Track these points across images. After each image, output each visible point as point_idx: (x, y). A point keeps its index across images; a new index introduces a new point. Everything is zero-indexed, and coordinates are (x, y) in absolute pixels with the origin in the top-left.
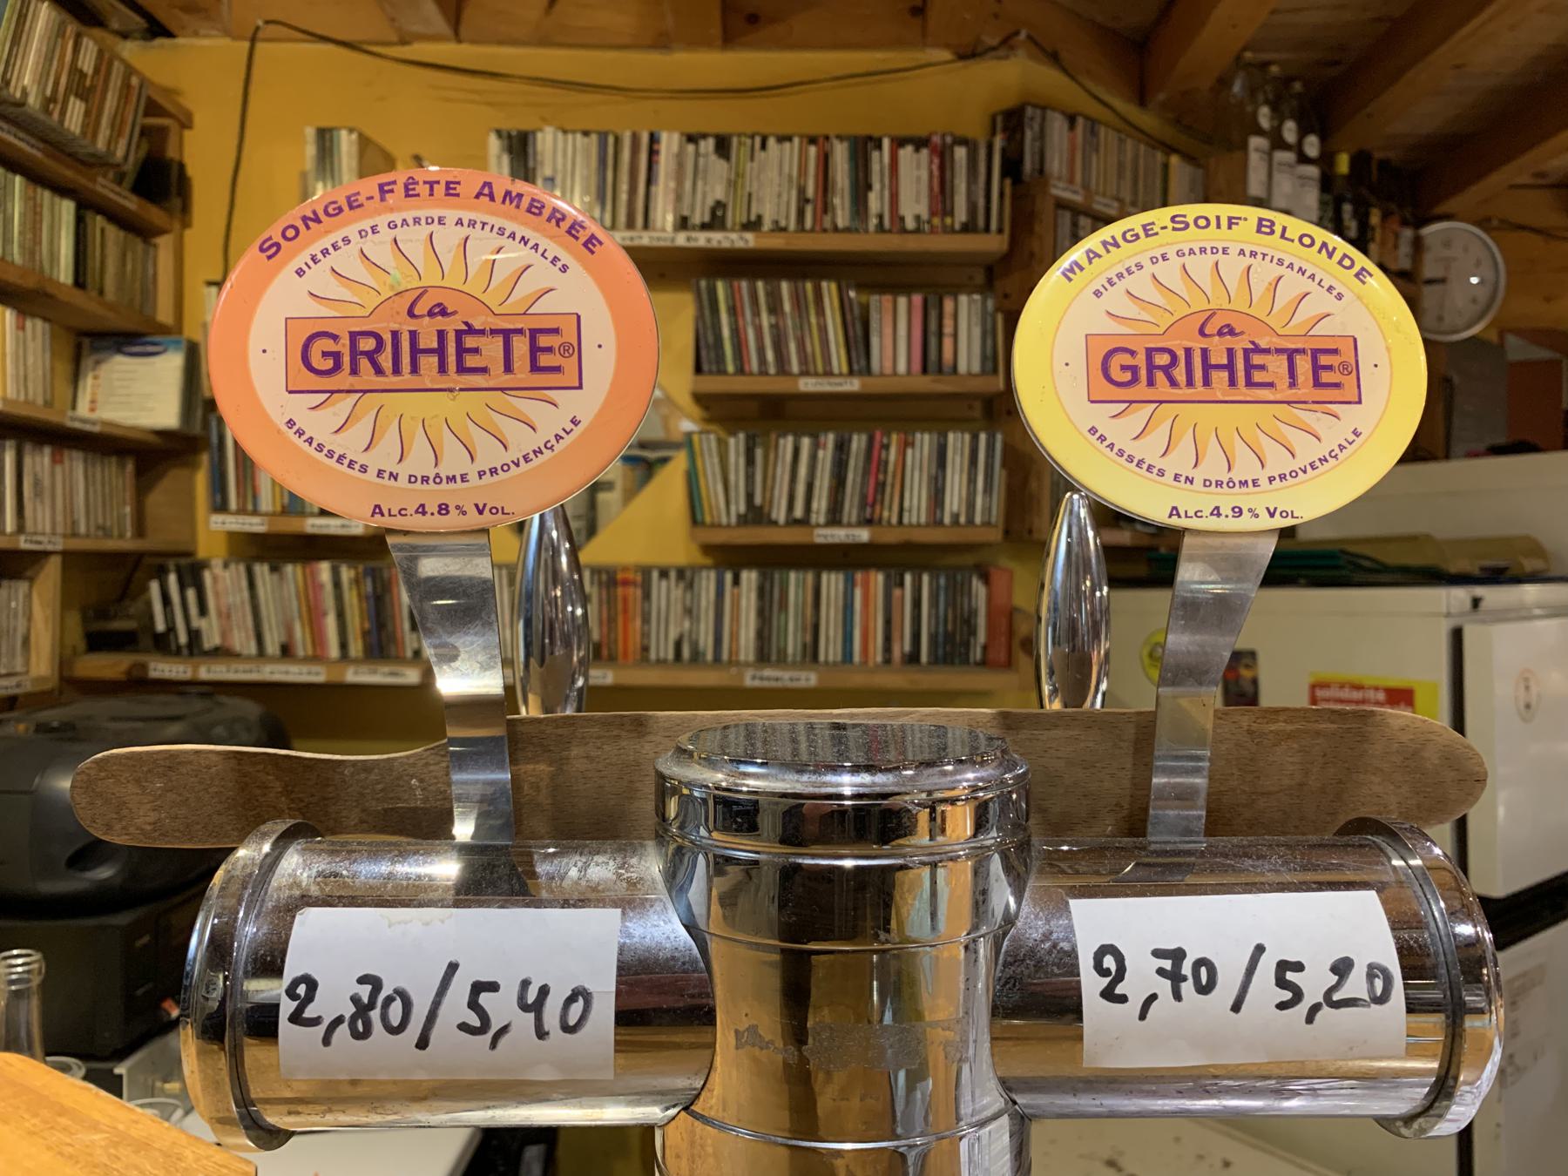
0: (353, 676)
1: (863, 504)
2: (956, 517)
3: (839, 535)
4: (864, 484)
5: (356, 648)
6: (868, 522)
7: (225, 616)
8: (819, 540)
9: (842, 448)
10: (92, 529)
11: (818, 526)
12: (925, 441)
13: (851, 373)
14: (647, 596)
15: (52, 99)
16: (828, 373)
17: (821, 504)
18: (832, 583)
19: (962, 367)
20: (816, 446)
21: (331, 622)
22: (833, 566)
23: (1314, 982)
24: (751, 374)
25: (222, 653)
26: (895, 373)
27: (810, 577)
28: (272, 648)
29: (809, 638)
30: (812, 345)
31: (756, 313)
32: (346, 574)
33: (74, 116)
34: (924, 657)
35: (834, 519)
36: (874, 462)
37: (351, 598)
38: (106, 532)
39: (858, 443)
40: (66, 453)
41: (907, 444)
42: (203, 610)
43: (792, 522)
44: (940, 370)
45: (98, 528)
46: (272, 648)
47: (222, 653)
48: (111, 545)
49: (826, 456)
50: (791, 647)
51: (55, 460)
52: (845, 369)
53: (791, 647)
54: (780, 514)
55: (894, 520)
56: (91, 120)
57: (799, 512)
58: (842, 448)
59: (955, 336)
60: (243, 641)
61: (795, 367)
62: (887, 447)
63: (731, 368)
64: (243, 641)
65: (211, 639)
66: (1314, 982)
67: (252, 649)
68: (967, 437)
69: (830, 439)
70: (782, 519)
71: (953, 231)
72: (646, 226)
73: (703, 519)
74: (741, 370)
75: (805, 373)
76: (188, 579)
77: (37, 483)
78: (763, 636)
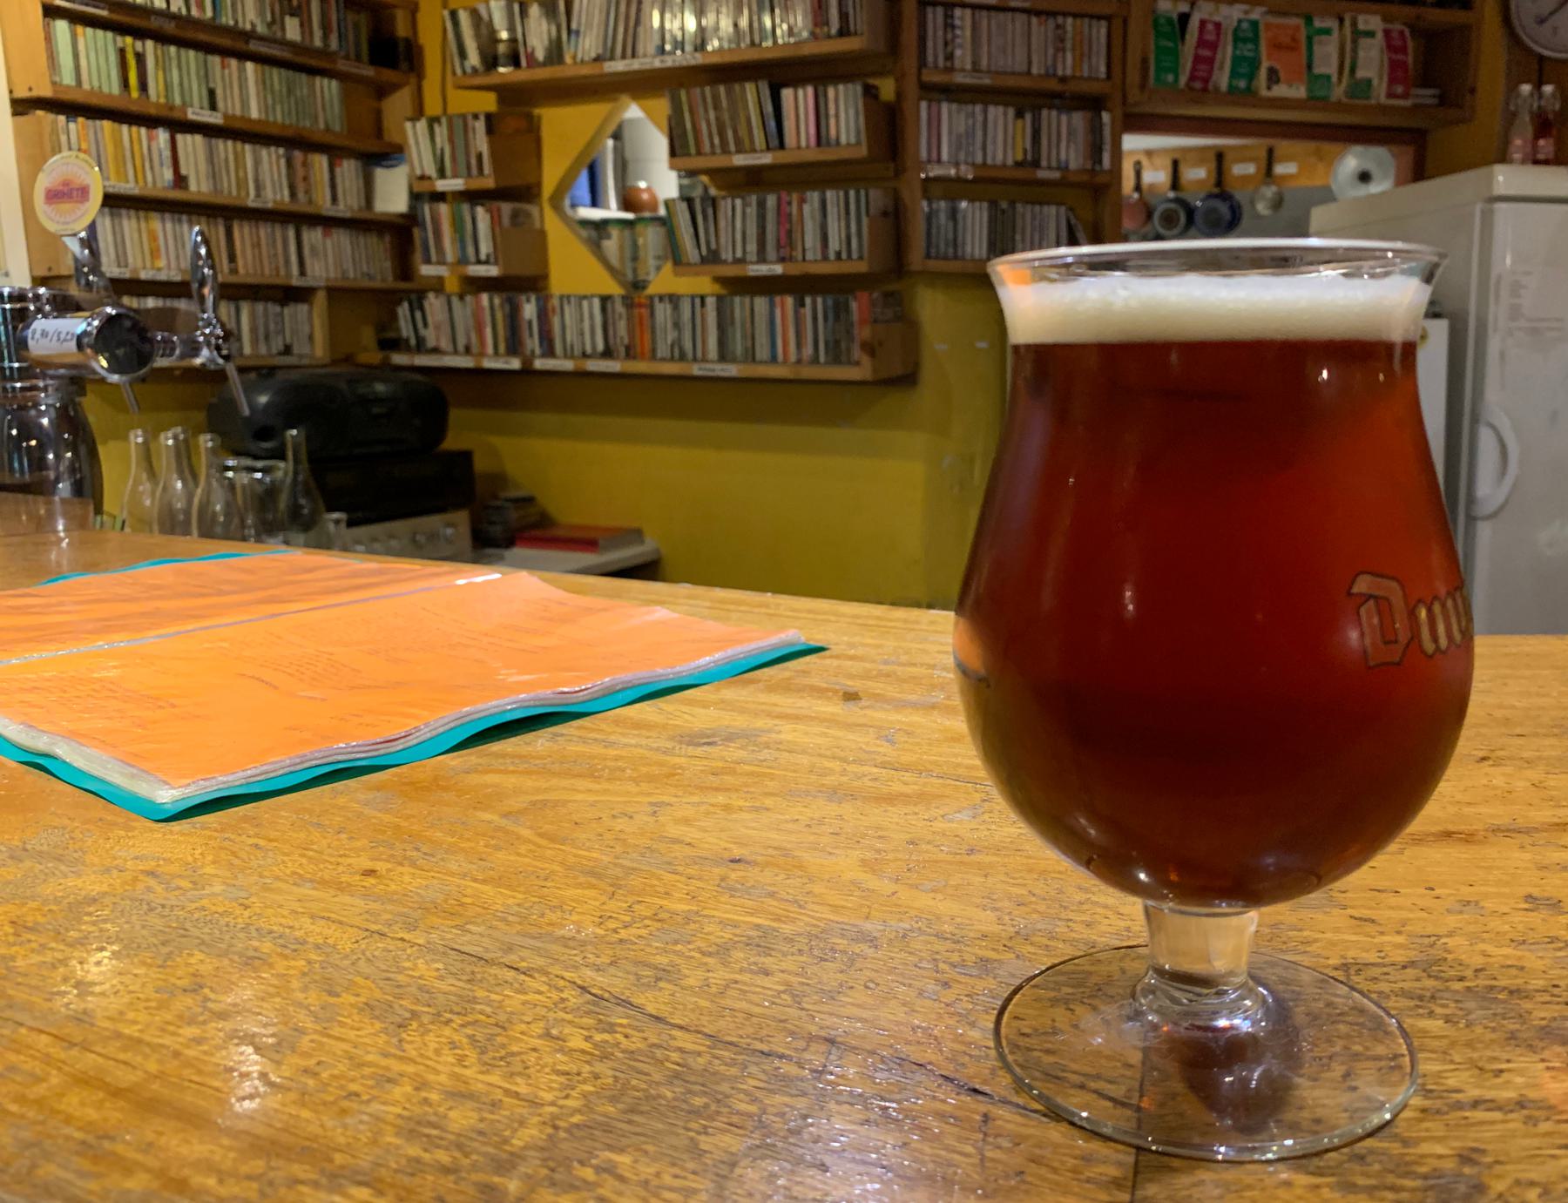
0: (488, 364)
1: (779, 247)
2: (838, 254)
3: (762, 270)
4: (778, 231)
5: (502, 348)
6: (782, 260)
7: (437, 328)
8: (751, 274)
9: (762, 205)
10: (359, 276)
11: (752, 263)
12: (814, 196)
13: (768, 149)
14: (652, 314)
15: (273, 22)
16: (754, 150)
17: (752, 247)
18: (761, 303)
19: (843, 140)
20: (745, 205)
21: (488, 331)
22: (762, 293)
23: (62, 336)
24: (705, 155)
25: (436, 351)
26: (799, 147)
27: (747, 300)
28: (461, 348)
29: (749, 344)
30: (743, 133)
31: (706, 110)
32: (497, 301)
33: (292, 30)
34: (822, 358)
35: (762, 259)
36: (783, 215)
37: (499, 316)
38: (371, 277)
39: (771, 200)
40: (334, 230)
41: (802, 201)
42: (426, 325)
43: (737, 261)
44: (828, 144)
45: (363, 274)
46: (461, 348)
47: (436, 351)
48: (377, 284)
49: (752, 211)
50: (739, 350)
51: (325, 235)
52: (764, 147)
53: (739, 350)
54: (726, 255)
55: (800, 257)
56: (305, 26)
57: (739, 254)
58: (762, 205)
59: (837, 116)
60: (445, 344)
61: (732, 147)
62: (790, 203)
63: (693, 150)
64: (445, 344)
65: (431, 343)
66: (62, 336)
67: (450, 348)
68: (841, 194)
69: (754, 199)
70: (730, 259)
71: (829, 37)
72: (634, 56)
73: (964, 252)
74: (699, 153)
75: (739, 151)
76: (415, 305)
77: (313, 249)
78: (722, 343)
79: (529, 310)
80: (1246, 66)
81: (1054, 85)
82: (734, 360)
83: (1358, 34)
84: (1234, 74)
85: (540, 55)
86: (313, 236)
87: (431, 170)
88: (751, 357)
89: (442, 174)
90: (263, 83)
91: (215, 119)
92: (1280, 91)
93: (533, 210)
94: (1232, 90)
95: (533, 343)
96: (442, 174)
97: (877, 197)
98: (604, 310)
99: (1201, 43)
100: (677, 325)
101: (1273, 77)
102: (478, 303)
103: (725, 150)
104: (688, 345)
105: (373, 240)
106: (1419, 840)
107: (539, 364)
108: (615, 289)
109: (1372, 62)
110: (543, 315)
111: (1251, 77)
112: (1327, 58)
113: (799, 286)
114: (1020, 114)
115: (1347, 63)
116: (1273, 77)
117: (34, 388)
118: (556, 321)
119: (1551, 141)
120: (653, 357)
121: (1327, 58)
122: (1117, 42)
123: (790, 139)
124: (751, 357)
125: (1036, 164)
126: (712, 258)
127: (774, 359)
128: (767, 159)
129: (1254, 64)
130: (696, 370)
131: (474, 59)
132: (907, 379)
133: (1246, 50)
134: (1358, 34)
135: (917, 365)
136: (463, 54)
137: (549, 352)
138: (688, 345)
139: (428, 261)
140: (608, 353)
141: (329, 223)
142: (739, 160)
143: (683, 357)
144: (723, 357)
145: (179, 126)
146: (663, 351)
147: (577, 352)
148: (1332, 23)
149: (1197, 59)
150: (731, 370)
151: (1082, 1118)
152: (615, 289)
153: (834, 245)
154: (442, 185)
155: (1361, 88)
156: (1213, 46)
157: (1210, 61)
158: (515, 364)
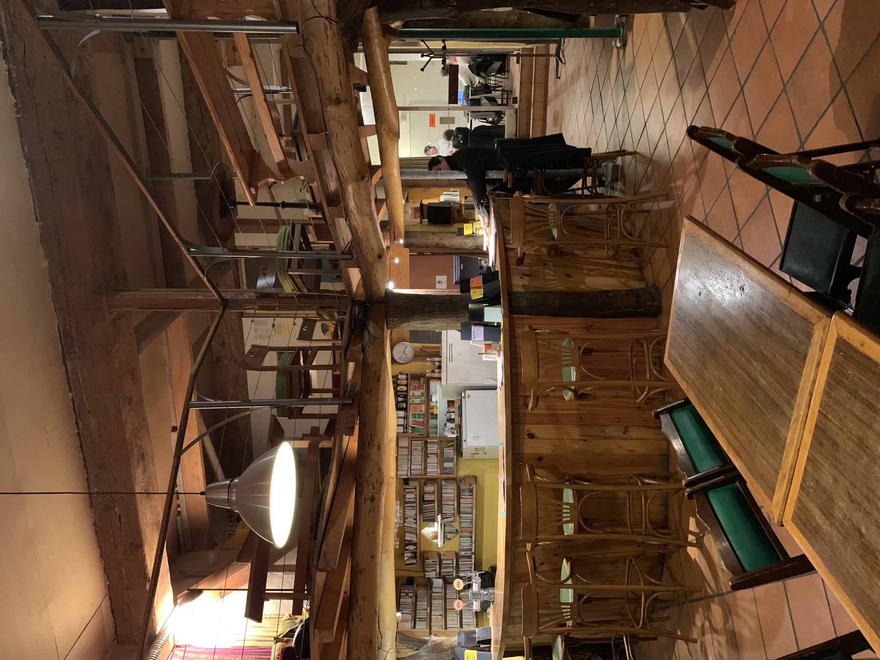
18: (462, 505)
22: (460, 505)
49: (445, 506)
54: (453, 512)
79: (463, 553)
80: (420, 416)
81: (423, 451)
82: (472, 511)
83: (413, 396)
84: (421, 418)
85: (415, 547)
86: (448, 596)
87: (435, 573)
88: (472, 508)
89: (436, 570)
90: (420, 601)
91: (429, 609)
92: (423, 410)
93: (442, 553)
94: (423, 418)
95: (469, 553)
96: (436, 570)
97: (443, 483)
98: (463, 537)
99: (416, 424)
100: (466, 522)
101: (421, 411)
102: (461, 564)
103: (434, 511)
104: (470, 520)
105: (447, 587)
106: (723, 160)
107: (473, 551)
108: (458, 536)
109: (418, 393)
110: (463, 550)
111: (421, 415)
112: (417, 401)
113: (459, 498)
114: (429, 457)
115: (419, 397)
116: (421, 411)
117: (488, 580)
118: (465, 548)
119: (572, 534)
120: (472, 527)
121: (417, 401)
122: (415, 439)
123: (433, 499)
124: (472, 508)
125: (437, 454)
126: (453, 514)
127: (472, 503)
128: (436, 503)
129: (419, 414)
130: (474, 518)
131: (414, 561)
132: (475, 477)
133: (417, 416)
134: (413, 396)
135: (473, 476)
136: (413, 564)
137: (471, 549)
138: (470, 520)
139: (452, 575)
140: (471, 537)
141: (445, 594)
142: (436, 509)
143: (472, 522)
144: (472, 514)
145: (431, 614)
146: (471, 526)
147: (470, 543)
148: (411, 400)
149: (419, 425)
150: (474, 511)
151: (852, 422)
152: (458, 536)
153: (452, 491)
154: (438, 571)
155: (422, 394)
156: (416, 422)
157: (419, 422)
158: (473, 556)
